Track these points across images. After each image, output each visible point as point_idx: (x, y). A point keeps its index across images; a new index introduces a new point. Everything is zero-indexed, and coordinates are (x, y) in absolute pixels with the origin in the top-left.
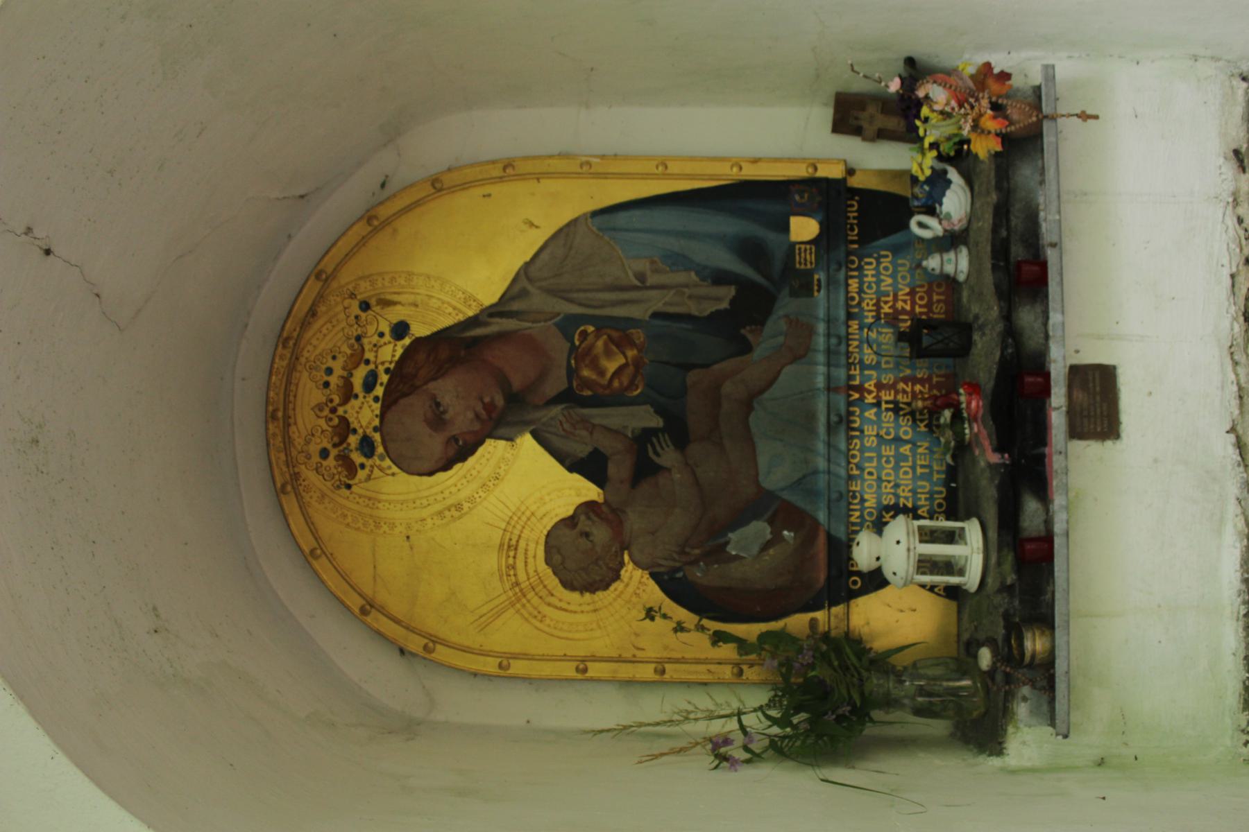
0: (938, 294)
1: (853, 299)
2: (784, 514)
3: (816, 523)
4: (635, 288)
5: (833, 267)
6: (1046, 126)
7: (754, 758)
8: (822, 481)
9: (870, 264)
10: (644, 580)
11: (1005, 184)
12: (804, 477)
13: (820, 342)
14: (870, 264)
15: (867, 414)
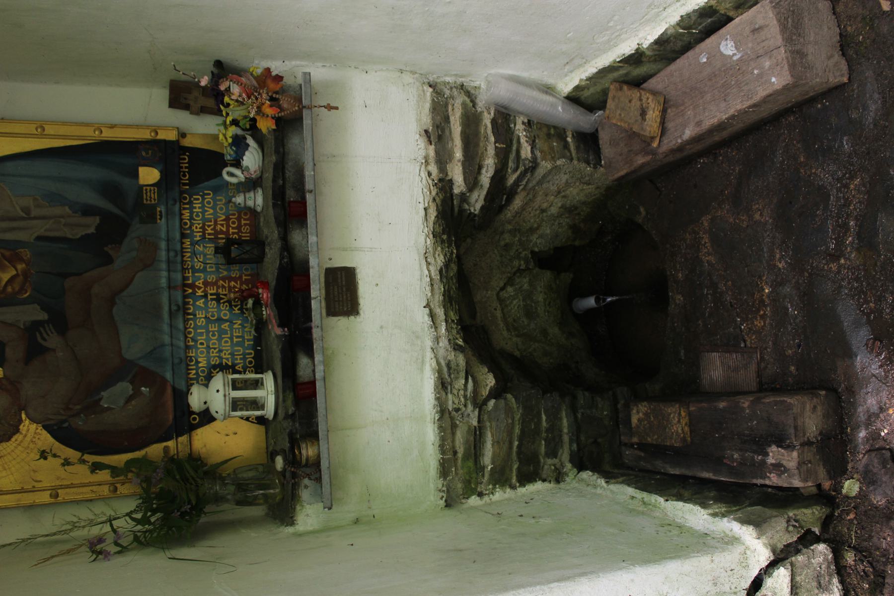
0: (245, 220)
1: (186, 224)
2: (142, 376)
3: (164, 381)
4: (23, 219)
5: (171, 202)
6: (305, 112)
7: (123, 550)
8: (168, 351)
9: (198, 199)
10: (38, 431)
11: (281, 150)
12: (155, 349)
13: (163, 254)
14: (198, 199)
15: (198, 303)
